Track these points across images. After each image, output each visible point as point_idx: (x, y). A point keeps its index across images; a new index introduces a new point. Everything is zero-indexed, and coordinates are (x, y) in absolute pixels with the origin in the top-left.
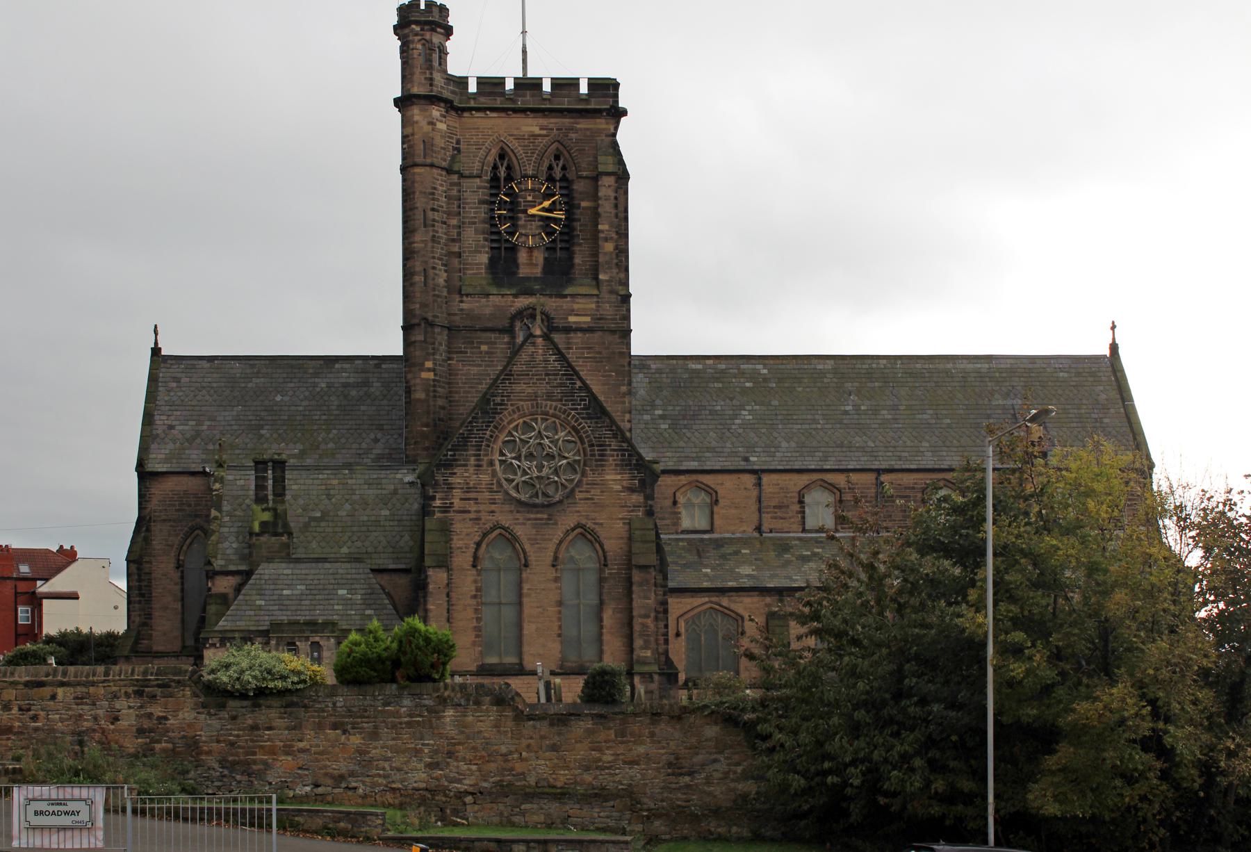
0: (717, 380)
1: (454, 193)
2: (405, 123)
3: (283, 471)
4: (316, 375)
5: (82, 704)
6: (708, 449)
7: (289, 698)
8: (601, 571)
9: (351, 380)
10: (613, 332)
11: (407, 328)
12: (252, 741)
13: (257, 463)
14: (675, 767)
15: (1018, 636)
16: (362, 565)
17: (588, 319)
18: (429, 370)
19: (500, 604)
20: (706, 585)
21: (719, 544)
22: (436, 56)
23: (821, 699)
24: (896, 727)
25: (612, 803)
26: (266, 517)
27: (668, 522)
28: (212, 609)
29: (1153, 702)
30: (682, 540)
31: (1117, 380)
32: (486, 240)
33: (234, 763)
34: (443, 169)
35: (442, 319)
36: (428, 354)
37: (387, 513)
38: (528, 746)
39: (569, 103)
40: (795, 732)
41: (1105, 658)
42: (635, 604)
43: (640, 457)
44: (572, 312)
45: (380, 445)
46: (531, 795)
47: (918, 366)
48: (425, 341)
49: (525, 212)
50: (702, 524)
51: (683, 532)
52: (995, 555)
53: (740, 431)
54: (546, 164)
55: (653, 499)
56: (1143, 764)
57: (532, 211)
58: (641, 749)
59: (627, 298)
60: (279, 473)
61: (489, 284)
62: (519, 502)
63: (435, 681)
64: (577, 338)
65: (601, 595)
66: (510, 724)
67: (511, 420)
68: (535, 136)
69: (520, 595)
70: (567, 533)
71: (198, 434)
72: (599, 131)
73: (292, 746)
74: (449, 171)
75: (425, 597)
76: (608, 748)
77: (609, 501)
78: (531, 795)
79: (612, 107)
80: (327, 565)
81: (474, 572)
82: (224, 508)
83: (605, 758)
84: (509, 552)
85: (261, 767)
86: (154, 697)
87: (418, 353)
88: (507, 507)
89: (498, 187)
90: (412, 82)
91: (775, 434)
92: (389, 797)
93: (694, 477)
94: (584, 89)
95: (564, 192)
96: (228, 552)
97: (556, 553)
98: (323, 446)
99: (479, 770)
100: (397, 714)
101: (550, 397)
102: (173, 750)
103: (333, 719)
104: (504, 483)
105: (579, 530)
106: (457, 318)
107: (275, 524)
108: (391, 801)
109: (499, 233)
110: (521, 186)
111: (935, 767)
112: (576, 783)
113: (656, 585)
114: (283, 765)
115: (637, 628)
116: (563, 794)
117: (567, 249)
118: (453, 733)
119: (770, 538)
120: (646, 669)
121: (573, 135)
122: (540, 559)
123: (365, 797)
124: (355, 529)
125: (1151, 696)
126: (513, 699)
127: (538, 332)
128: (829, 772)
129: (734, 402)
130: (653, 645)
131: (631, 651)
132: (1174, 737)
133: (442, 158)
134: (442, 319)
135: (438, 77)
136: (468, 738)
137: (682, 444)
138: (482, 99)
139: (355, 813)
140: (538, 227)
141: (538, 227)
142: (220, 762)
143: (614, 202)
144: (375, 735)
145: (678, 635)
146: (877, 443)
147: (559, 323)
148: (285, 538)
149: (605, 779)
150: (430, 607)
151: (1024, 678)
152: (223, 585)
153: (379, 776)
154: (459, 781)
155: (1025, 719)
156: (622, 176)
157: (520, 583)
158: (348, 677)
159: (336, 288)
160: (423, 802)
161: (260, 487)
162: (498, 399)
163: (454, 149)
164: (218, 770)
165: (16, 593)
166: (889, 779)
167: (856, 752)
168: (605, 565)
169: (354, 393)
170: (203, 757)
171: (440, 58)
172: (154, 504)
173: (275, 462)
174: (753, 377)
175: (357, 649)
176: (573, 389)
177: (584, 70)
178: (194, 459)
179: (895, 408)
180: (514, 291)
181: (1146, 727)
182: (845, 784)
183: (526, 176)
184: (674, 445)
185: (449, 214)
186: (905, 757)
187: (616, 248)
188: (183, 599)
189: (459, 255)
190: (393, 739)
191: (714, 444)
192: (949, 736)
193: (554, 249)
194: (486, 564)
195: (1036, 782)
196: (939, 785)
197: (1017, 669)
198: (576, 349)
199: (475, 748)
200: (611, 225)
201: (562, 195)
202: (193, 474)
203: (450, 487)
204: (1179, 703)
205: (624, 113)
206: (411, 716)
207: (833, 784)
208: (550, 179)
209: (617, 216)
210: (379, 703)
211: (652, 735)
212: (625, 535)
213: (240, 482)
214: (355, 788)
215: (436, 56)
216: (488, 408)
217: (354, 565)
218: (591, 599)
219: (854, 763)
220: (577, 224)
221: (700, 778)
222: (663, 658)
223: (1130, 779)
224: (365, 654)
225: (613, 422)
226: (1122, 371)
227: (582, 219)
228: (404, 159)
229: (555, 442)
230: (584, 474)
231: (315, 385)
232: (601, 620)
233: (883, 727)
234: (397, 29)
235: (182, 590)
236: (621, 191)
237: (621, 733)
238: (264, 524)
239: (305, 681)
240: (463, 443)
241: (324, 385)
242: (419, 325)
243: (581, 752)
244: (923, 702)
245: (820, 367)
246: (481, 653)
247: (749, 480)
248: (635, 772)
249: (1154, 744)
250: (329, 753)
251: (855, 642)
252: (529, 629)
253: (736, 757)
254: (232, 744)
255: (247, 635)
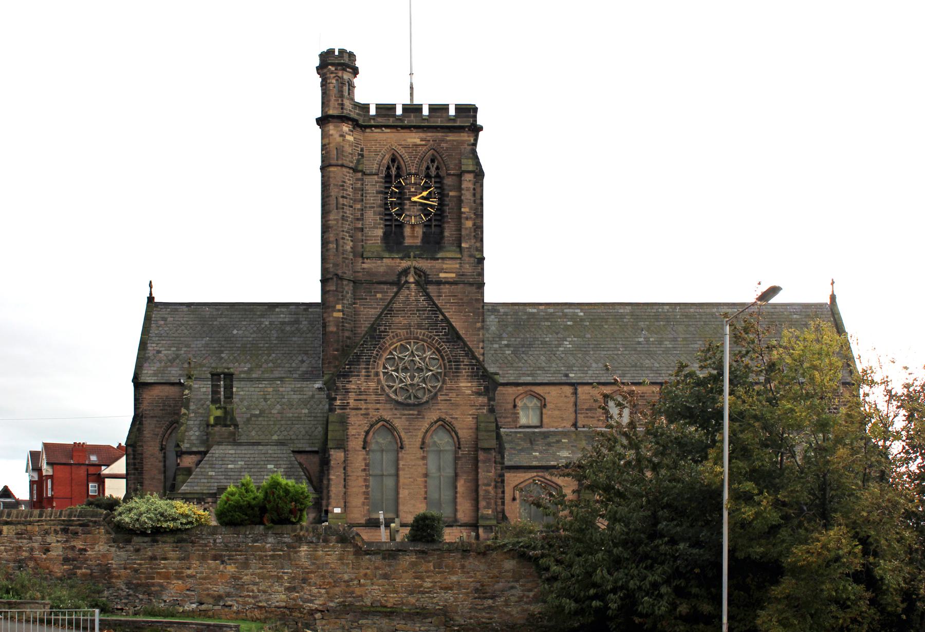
0: (547, 320)
1: (359, 185)
2: (324, 136)
3: (232, 381)
4: (262, 316)
5: (21, 538)
6: (539, 368)
7: (179, 536)
8: (456, 452)
9: (287, 320)
10: (471, 284)
11: (324, 281)
12: (151, 568)
13: (213, 375)
14: (481, 592)
15: (749, 486)
16: (285, 448)
17: (453, 275)
18: (339, 311)
19: (382, 475)
20: (535, 463)
21: (546, 435)
22: (346, 88)
23: (591, 539)
24: (649, 561)
25: (430, 620)
26: (219, 413)
27: (509, 420)
28: (180, 478)
29: (864, 541)
30: (520, 432)
31: (835, 320)
32: (381, 219)
33: (139, 585)
34: (350, 168)
35: (349, 274)
36: (338, 299)
37: (306, 411)
38: (366, 575)
39: (441, 122)
40: (570, 566)
41: (823, 504)
42: (480, 475)
43: (485, 370)
44: (442, 270)
45: (305, 365)
46: (366, 612)
47: (692, 310)
48: (336, 291)
49: (409, 199)
50: (534, 421)
51: (520, 427)
52: (731, 419)
53: (563, 356)
54: (424, 168)
55: (494, 400)
56: (855, 594)
57: (415, 199)
58: (454, 578)
59: (481, 260)
60: (228, 382)
61: (384, 251)
62: (397, 402)
63: (293, 523)
64: (446, 289)
65: (456, 469)
66: (351, 557)
67: (391, 343)
68: (417, 145)
69: (397, 469)
70: (431, 425)
71: (178, 356)
72: (463, 142)
73: (182, 573)
74: (355, 170)
75: (328, 470)
76: (428, 577)
77: (462, 401)
78: (366, 612)
79: (472, 124)
80: (260, 447)
81: (364, 452)
82: (191, 408)
83: (425, 585)
84: (389, 438)
85: (159, 588)
86: (77, 533)
87: (331, 299)
88: (388, 406)
89: (391, 182)
90: (328, 106)
91: (588, 358)
92: (257, 613)
93: (529, 388)
94: (452, 112)
95: (438, 185)
96: (192, 438)
97: (424, 438)
98: (264, 366)
99: (327, 593)
100: (263, 549)
101: (420, 326)
102: (91, 575)
103: (213, 552)
104: (386, 388)
105: (440, 423)
106: (360, 274)
107: (225, 418)
108: (258, 616)
109: (391, 215)
110: (405, 181)
111: (680, 592)
112: (403, 603)
113: (495, 462)
114: (174, 589)
115: (481, 493)
116: (392, 613)
117: (439, 226)
118: (307, 564)
119: (583, 432)
120: (488, 523)
121: (444, 145)
122: (412, 443)
123: (238, 612)
124: (283, 422)
125: (862, 534)
126: (353, 538)
127: (412, 280)
128: (593, 598)
129: (560, 335)
130: (493, 506)
131: (477, 509)
132: (884, 569)
133: (351, 161)
134: (349, 274)
135: (347, 103)
136: (318, 568)
137: (521, 364)
138: (379, 120)
139: (214, 626)
140: (418, 210)
141: (418, 210)
142: (127, 584)
143: (472, 191)
144: (246, 565)
145: (514, 499)
146: (662, 364)
147: (432, 278)
148: (232, 428)
149: (425, 601)
150: (332, 477)
151: (753, 520)
152: (188, 461)
153: (249, 596)
154: (311, 601)
155: (754, 556)
156: (479, 174)
157: (397, 460)
158: (225, 519)
159: (276, 258)
160: (283, 617)
161: (215, 392)
162: (382, 328)
163: (359, 154)
164: (125, 590)
165: (88, 474)
166: (642, 603)
167: (616, 581)
168: (459, 448)
169: (288, 328)
170: (114, 580)
171: (349, 89)
172: (145, 405)
173: (225, 374)
174: (574, 317)
175: (233, 498)
176: (437, 320)
177: (452, 99)
178: (174, 373)
179: (674, 340)
180: (400, 255)
181: (857, 564)
182: (607, 608)
183: (410, 174)
184: (515, 365)
185: (355, 201)
186: (655, 585)
187: (474, 224)
188: (165, 472)
189: (362, 230)
190: (261, 568)
191: (543, 364)
192: (693, 569)
193: (430, 226)
194: (373, 446)
195: (762, 608)
196: (683, 608)
197: (748, 512)
198: (444, 298)
199: (323, 576)
200: (471, 209)
201: (436, 188)
202: (173, 384)
203: (347, 392)
204: (887, 540)
205: (481, 128)
206: (274, 550)
207: (596, 607)
208: (428, 176)
209: (475, 202)
210: (249, 540)
211: (463, 567)
212: (474, 426)
213: (203, 389)
214: (231, 606)
215: (346, 88)
216: (375, 334)
217: (279, 447)
218: (449, 472)
219: (614, 590)
220: (446, 208)
221: (500, 601)
222: (500, 515)
223: (843, 605)
224: (238, 502)
225: (465, 344)
226: (839, 314)
227: (450, 204)
228: (323, 161)
229: (423, 359)
230: (444, 382)
231: (261, 323)
232: (456, 487)
233: (640, 561)
234: (319, 69)
235: (165, 466)
236: (479, 185)
237: (438, 565)
238: (217, 418)
239: (191, 523)
240: (357, 360)
241: (267, 323)
242: (332, 279)
243: (407, 580)
244: (673, 542)
245: (622, 311)
246: (368, 510)
247: (568, 390)
248: (449, 596)
249: (867, 577)
250: (210, 578)
251: (620, 494)
252: (403, 493)
253: (530, 584)
254: (136, 571)
255: (200, 496)
